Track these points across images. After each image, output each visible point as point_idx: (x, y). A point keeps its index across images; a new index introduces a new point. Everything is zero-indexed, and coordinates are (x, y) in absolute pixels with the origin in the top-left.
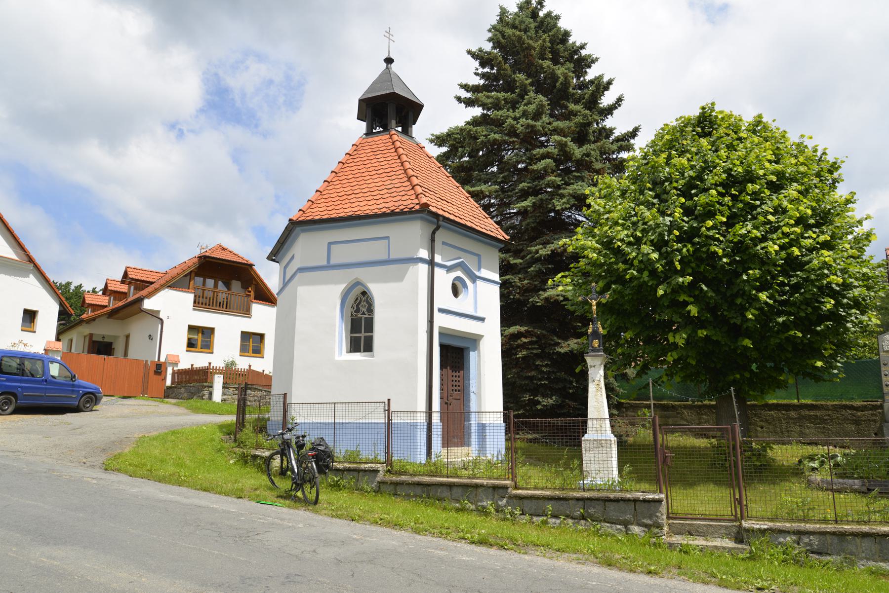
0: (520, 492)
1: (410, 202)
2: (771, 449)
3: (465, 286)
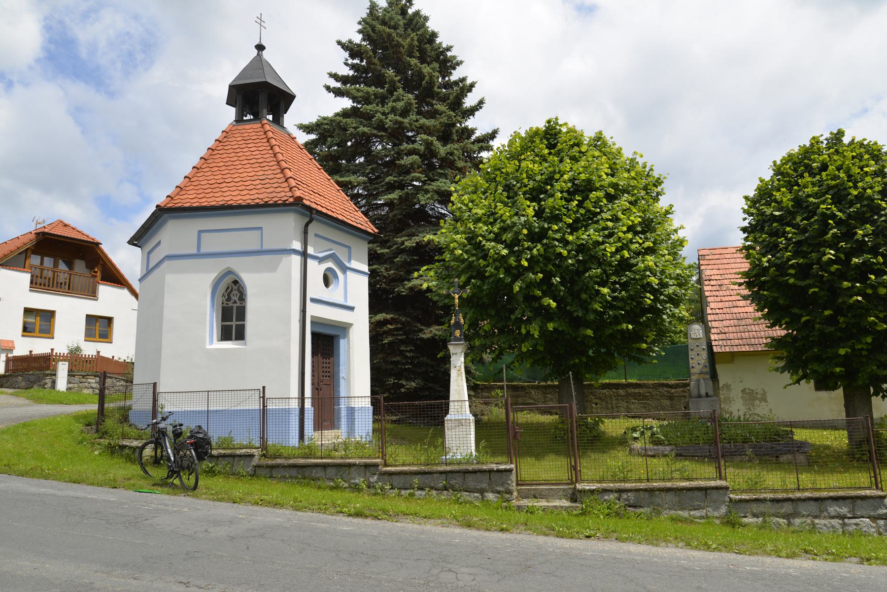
0: (389, 468)
1: (283, 194)
2: (603, 422)
3: (336, 277)
